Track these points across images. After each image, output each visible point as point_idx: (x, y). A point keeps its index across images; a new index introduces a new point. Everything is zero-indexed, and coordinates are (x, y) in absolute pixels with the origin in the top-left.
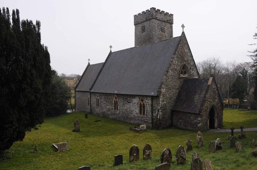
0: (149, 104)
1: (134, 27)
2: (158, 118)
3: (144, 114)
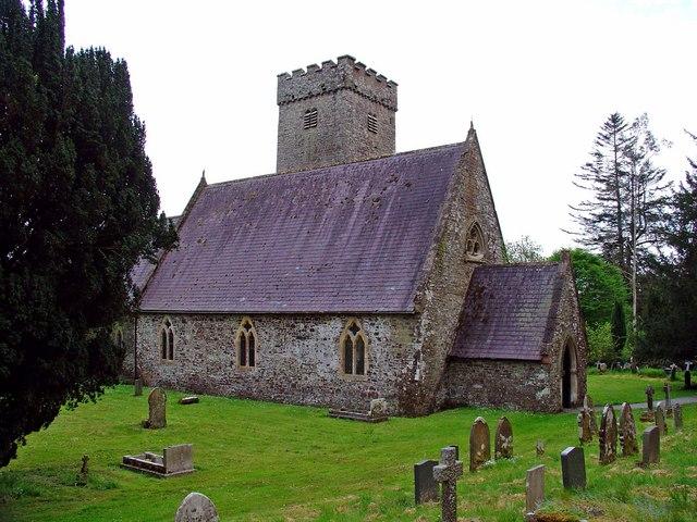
0: (379, 339)
1: (273, 112)
2: (417, 378)
3: (360, 370)
